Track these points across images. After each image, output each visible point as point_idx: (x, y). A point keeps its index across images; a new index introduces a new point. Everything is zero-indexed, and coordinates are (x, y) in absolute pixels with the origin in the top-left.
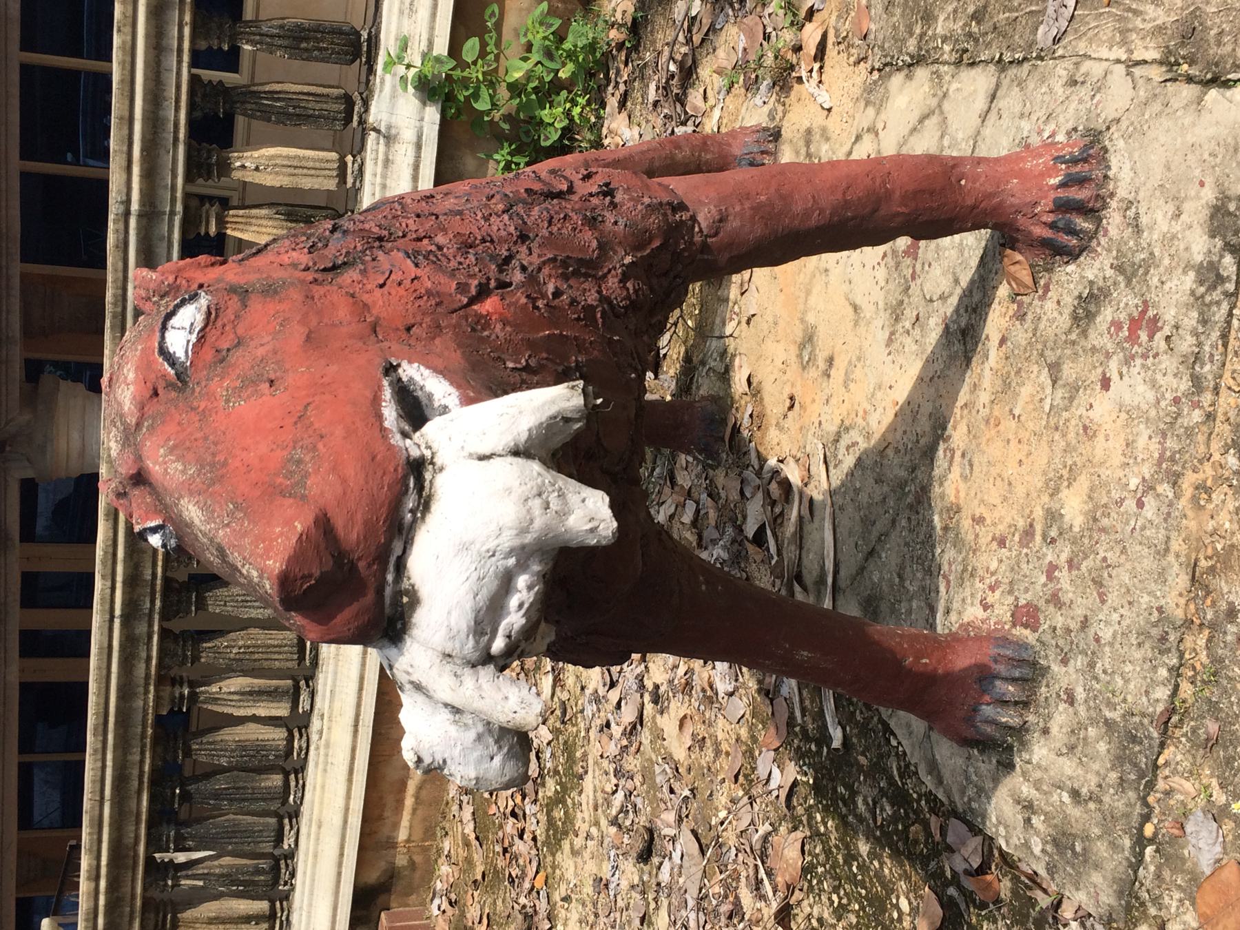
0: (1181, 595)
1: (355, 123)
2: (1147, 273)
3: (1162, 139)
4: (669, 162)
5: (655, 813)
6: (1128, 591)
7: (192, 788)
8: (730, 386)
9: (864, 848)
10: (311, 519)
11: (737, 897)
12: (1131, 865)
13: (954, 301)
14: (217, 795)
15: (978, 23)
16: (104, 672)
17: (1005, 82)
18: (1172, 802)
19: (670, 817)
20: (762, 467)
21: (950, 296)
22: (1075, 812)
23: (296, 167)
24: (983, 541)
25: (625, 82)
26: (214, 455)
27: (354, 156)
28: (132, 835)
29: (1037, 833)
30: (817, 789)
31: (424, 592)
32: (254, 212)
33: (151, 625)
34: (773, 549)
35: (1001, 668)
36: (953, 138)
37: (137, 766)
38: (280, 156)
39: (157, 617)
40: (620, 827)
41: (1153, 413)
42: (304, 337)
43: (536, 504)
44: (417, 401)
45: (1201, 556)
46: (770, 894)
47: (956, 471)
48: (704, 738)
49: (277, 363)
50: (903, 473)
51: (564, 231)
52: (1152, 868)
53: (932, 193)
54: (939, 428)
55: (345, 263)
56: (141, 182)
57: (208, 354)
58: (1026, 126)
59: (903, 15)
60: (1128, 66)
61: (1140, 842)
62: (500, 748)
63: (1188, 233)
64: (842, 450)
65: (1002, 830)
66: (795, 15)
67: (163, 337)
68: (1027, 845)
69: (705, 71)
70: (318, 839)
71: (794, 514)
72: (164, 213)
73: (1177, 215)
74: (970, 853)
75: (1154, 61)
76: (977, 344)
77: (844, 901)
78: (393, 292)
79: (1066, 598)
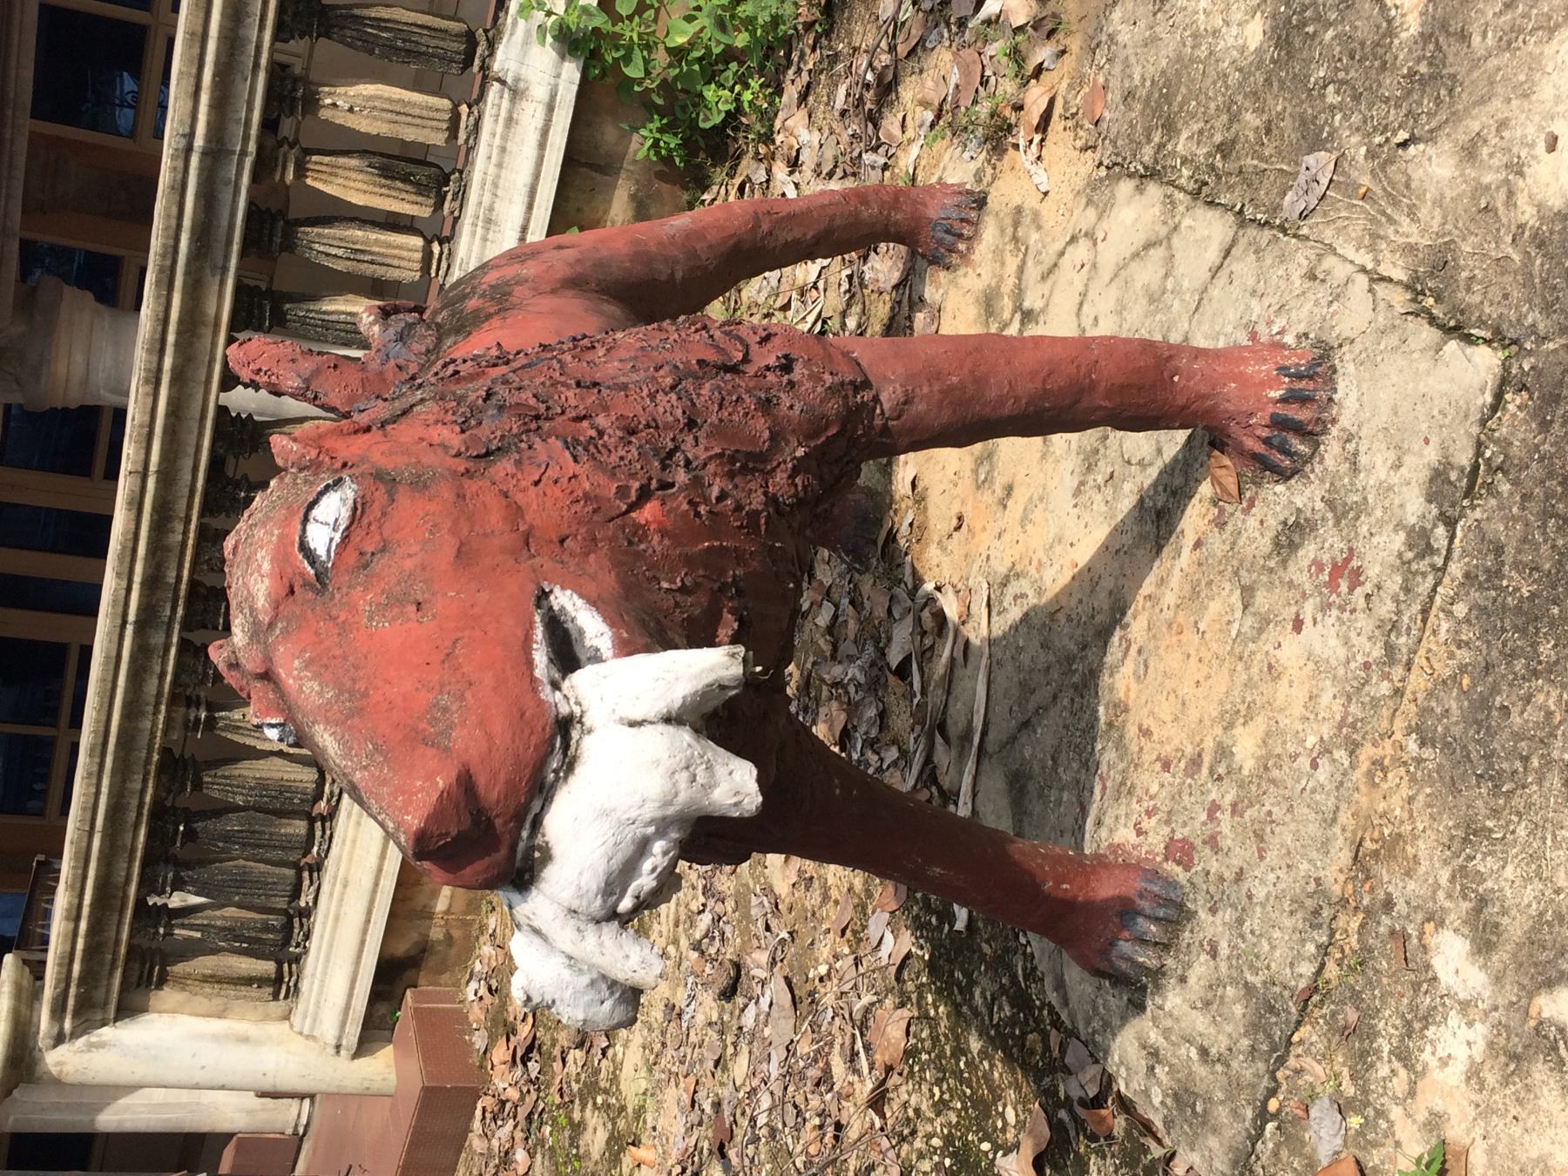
0: (1341, 871)
1: (476, 68)
2: (1357, 518)
3: (1395, 379)
4: (852, 220)
5: (744, 949)
6: (1289, 853)
7: (199, 825)
8: (891, 482)
9: (975, 1045)
10: (454, 775)
11: (828, 1064)
12: (1249, 1137)
13: (1153, 472)
14: (228, 838)
15: (1224, 157)
16: (109, 685)
17: (1243, 242)
18: (1300, 1082)
19: (763, 957)
20: (916, 588)
21: (1150, 464)
22: (1201, 1070)
23: (399, 112)
24: (1148, 757)
25: (810, 71)
26: (354, 680)
27: (470, 107)
28: (123, 873)
29: (1159, 1084)
30: (932, 967)
31: (557, 850)
32: (342, 160)
33: (169, 635)
34: (917, 686)
35: (1145, 905)
36: (1178, 284)
37: (137, 796)
38: (380, 97)
39: (177, 627)
40: (703, 953)
41: (1341, 671)
42: (453, 552)
43: (683, 777)
44: (566, 632)
45: (1367, 836)
46: (866, 1070)
47: (1128, 669)
48: (811, 878)
49: (425, 582)
50: (1072, 647)
51: (735, 418)
52: (1270, 1145)
53: (1140, 388)
54: (1118, 611)
55: (499, 449)
56: (209, 114)
57: (351, 557)
58: (1257, 308)
59: (1142, 114)
60: (1372, 280)
61: (1263, 1116)
62: (612, 993)
63: (1405, 489)
64: (1008, 599)
65: (1123, 1070)
66: (1020, 67)
67: (304, 530)
68: (1146, 1093)
69: (908, 92)
70: (341, 900)
71: (946, 653)
72: (234, 152)
73: (1397, 466)
74: (1084, 1084)
75: (1399, 282)
76: (1171, 533)
77: (946, 1097)
78: (549, 492)
79: (1226, 843)
